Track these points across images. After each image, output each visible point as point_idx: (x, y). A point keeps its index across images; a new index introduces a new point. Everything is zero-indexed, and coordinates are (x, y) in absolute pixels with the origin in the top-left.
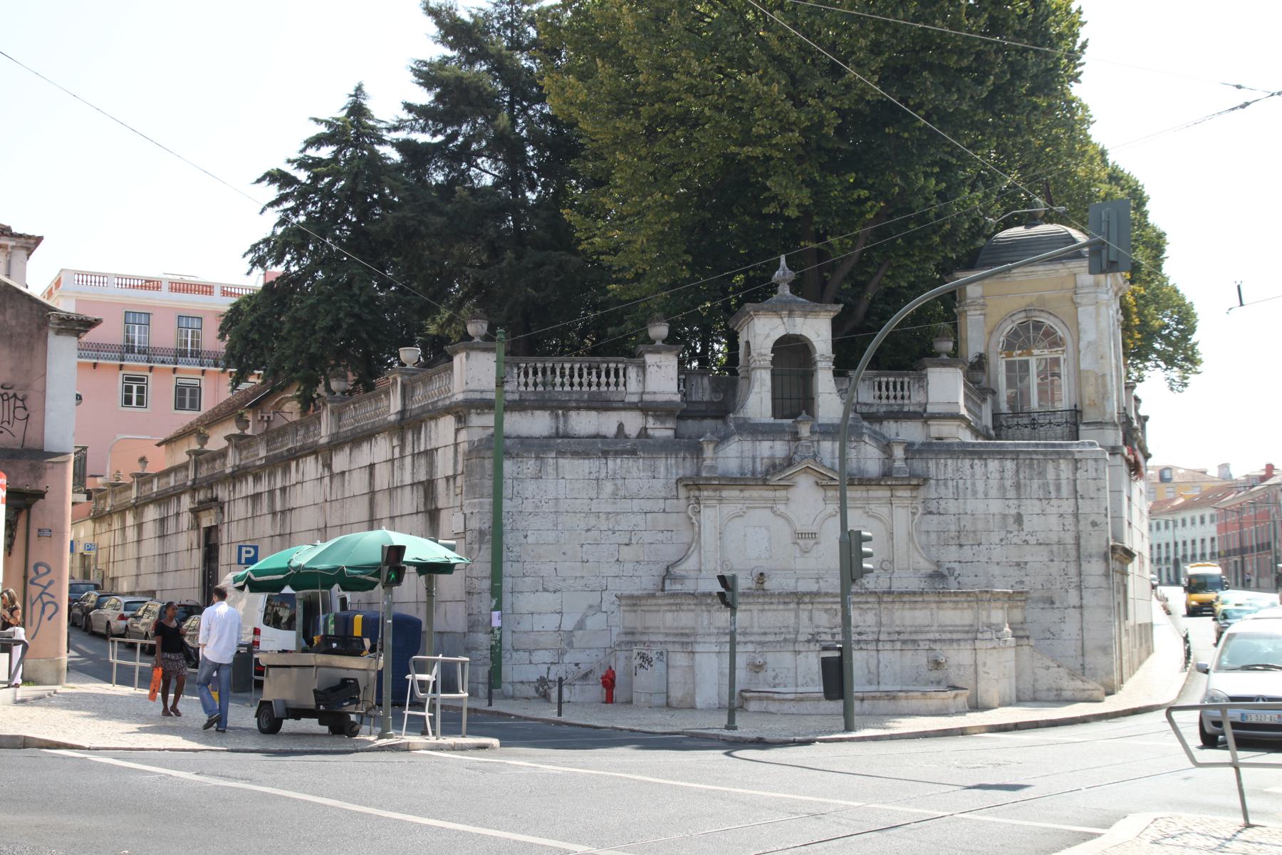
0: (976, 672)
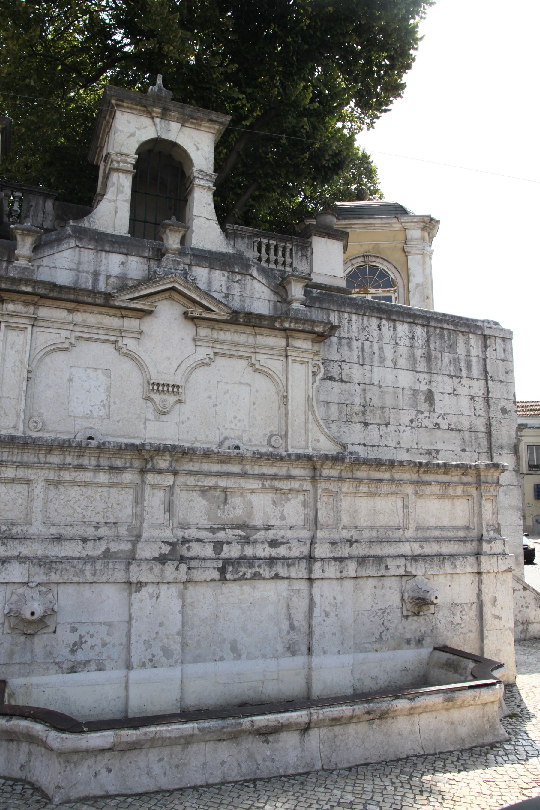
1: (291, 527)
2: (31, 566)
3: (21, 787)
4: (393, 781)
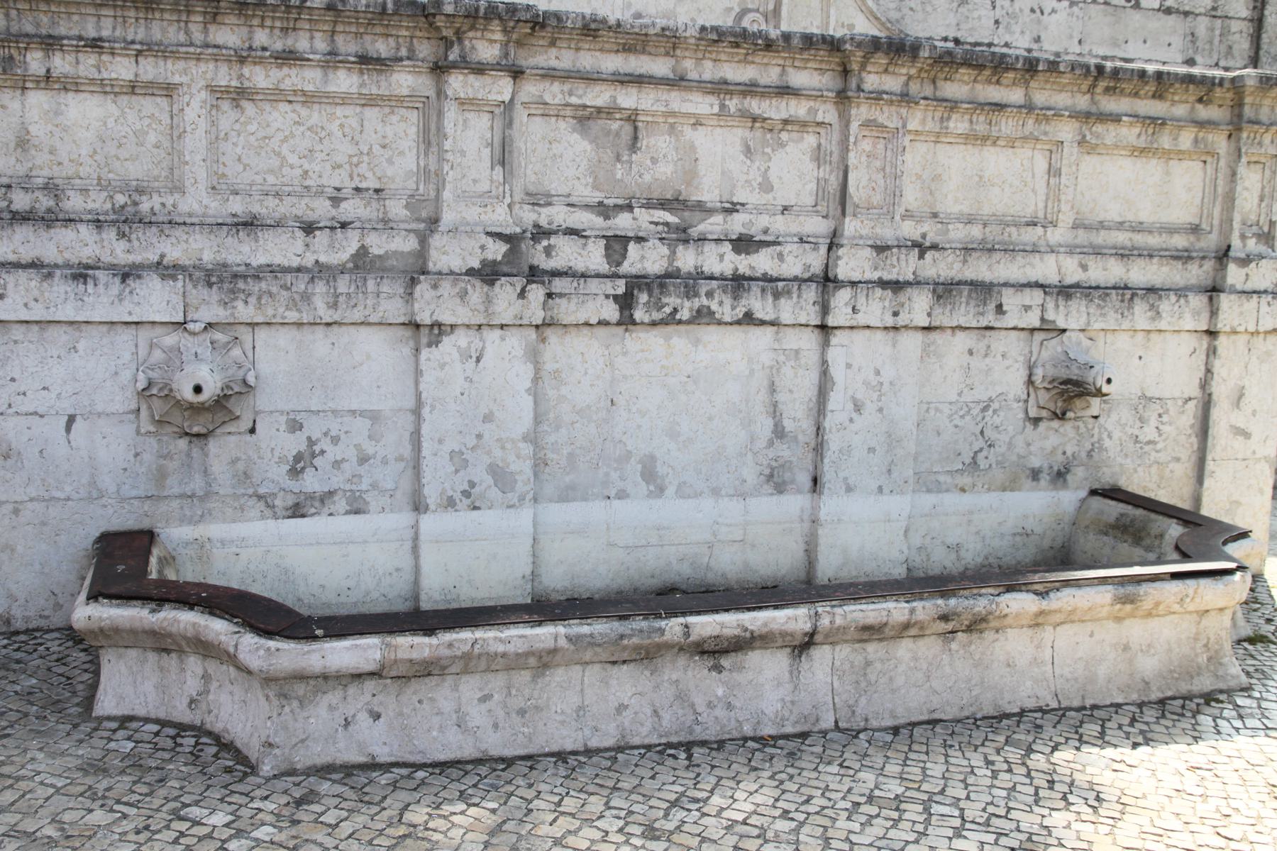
0: (1204, 429)
1: (785, 209)
2: (189, 286)
3: (192, 741)
4: (990, 758)
